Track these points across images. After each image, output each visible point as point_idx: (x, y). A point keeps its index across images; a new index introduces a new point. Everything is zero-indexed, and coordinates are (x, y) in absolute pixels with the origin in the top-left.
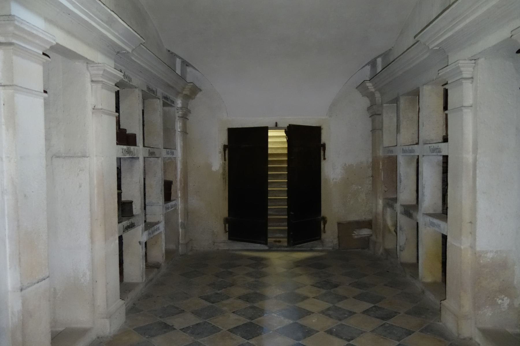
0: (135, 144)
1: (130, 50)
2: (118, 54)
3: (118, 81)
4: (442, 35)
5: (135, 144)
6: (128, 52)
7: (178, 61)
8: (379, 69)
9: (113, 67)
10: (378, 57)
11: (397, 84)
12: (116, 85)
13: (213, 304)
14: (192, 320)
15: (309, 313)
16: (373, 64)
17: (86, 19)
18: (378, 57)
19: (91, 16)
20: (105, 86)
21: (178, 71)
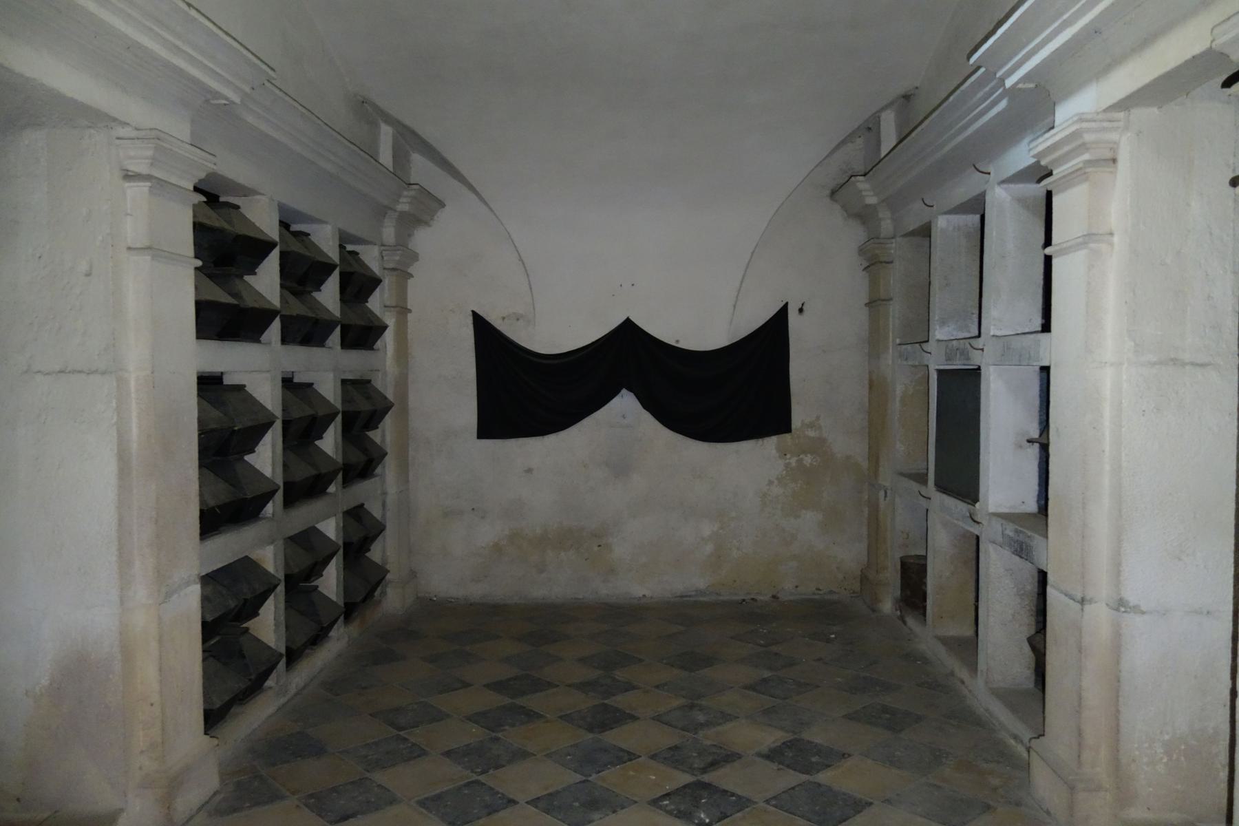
0: (940, 372)
1: (236, 98)
2: (211, 113)
3: (203, 175)
4: (965, 127)
5: (940, 372)
6: (233, 103)
7: (386, 133)
8: (889, 138)
9: (187, 138)
10: (883, 109)
11: (919, 176)
12: (196, 189)
13: (475, 777)
14: (450, 775)
15: (773, 755)
16: (871, 128)
17: (164, 53)
18: (883, 109)
19: (191, 56)
20: (159, 185)
21: (386, 157)
